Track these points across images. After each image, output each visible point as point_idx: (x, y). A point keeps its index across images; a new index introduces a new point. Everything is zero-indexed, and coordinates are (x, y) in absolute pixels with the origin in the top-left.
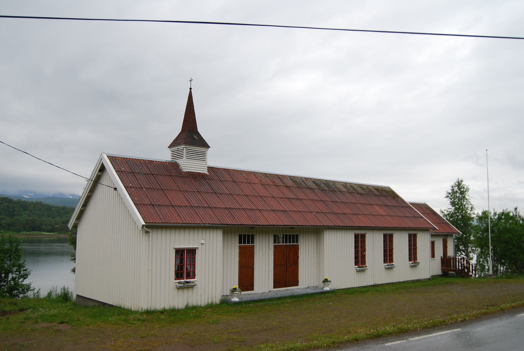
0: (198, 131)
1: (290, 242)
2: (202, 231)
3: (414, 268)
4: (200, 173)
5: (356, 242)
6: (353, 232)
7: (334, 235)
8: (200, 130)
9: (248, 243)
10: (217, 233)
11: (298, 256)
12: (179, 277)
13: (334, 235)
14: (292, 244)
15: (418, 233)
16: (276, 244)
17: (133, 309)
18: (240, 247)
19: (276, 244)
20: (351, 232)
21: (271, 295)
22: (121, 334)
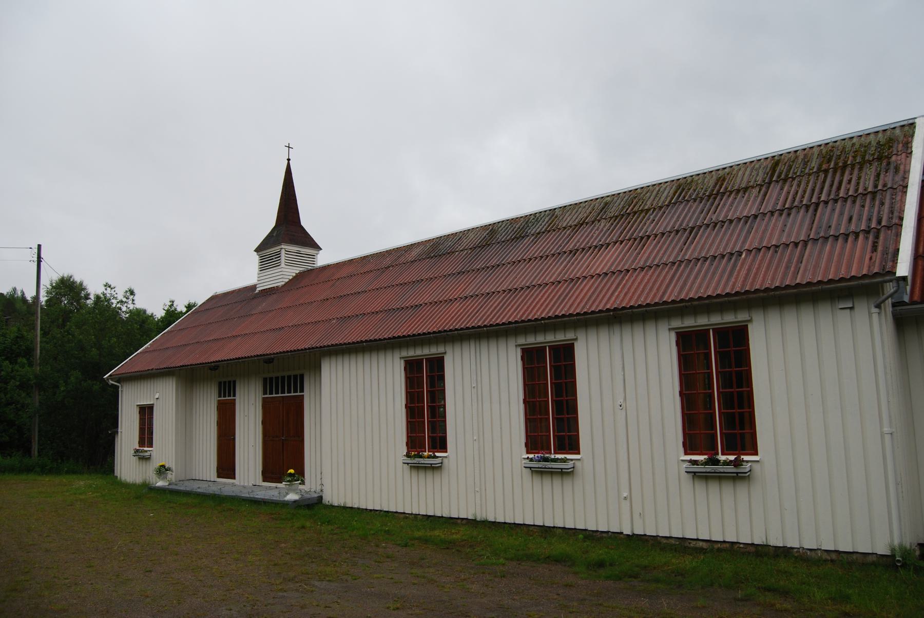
0: (303, 224)
1: (289, 392)
2: (393, 353)
3: (144, 462)
4: (274, 287)
5: (685, 362)
6: (512, 343)
7: (211, 388)
8: (304, 222)
9: (229, 396)
10: (855, 300)
11: (217, 425)
12: (553, 452)
13: (211, 388)
14: (292, 394)
15: (449, 349)
16: (266, 396)
17: (478, 519)
18: (265, 403)
19: (266, 396)
20: (389, 355)
21: (202, 488)
22: (125, 497)
